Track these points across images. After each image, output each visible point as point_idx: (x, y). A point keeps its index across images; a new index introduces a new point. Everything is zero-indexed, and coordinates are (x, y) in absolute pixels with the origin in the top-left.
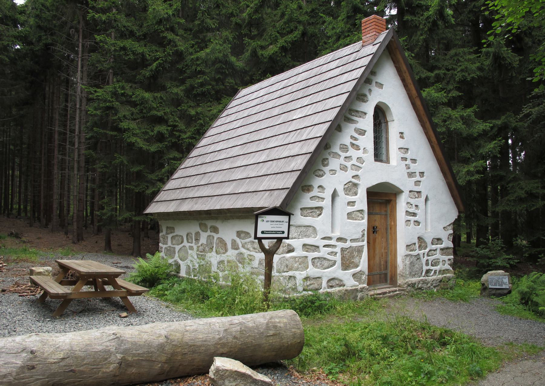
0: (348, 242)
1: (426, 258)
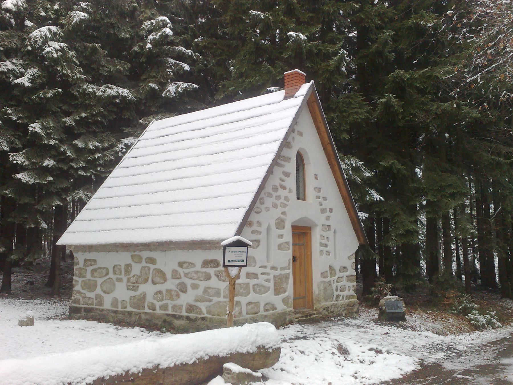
0: (279, 270)
1: (336, 284)
